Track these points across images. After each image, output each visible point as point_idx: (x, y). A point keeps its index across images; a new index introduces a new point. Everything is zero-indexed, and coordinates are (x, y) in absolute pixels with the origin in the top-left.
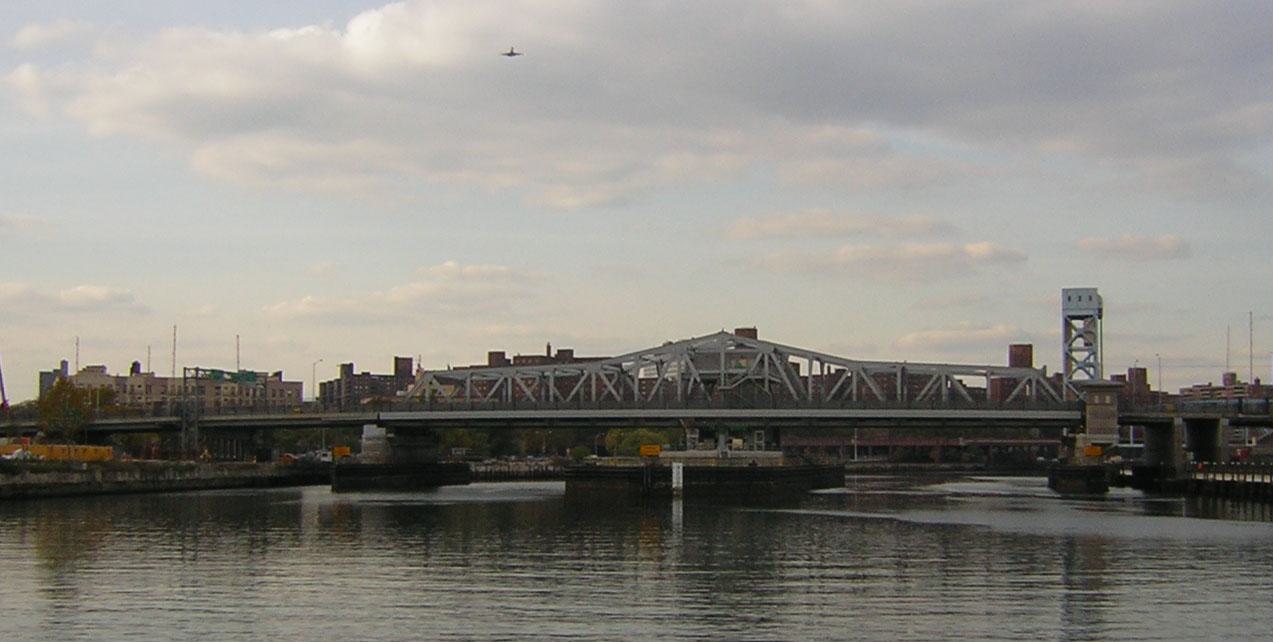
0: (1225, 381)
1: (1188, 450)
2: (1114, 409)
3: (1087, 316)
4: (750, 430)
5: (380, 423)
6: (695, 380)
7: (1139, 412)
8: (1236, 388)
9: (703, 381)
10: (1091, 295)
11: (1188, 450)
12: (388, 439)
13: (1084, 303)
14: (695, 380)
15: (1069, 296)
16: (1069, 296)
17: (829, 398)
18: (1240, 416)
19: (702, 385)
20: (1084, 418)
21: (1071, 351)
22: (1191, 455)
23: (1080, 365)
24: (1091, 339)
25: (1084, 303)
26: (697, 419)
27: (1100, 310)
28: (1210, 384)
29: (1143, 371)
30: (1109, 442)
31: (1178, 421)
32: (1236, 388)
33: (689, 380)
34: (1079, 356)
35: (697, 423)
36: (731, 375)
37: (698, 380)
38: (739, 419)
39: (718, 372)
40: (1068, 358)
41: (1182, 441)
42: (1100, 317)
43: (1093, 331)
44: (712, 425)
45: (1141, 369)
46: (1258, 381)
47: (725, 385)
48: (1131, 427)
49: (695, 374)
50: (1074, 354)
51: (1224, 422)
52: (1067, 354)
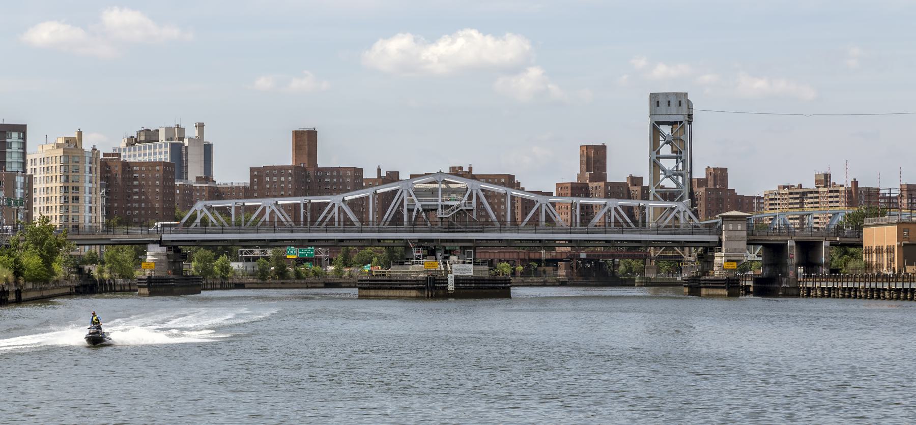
0: (818, 182)
1: (798, 265)
2: (744, 234)
3: (676, 123)
4: (464, 248)
5: (161, 243)
6: (418, 210)
7: (761, 235)
8: (831, 192)
9: (424, 210)
10: (682, 100)
11: (798, 265)
12: (168, 255)
13: (674, 107)
14: (418, 210)
15: (656, 100)
16: (656, 100)
17: (524, 223)
18: (838, 239)
19: (423, 214)
20: (720, 241)
21: (658, 158)
22: (800, 270)
23: (667, 174)
24: (681, 149)
25: (674, 107)
26: (420, 240)
27: (690, 116)
28: (800, 186)
29: (724, 171)
30: (741, 259)
31: (791, 243)
32: (831, 192)
33: (413, 210)
34: (669, 164)
35: (420, 244)
36: (447, 207)
37: (421, 210)
38: (453, 241)
39: (435, 203)
40: (656, 166)
41: (793, 256)
42: (690, 123)
43: (682, 138)
44: (432, 245)
45: (721, 169)
46: (855, 183)
47: (442, 214)
48: (752, 246)
49: (418, 205)
50: (663, 162)
51: (825, 244)
52: (654, 162)
